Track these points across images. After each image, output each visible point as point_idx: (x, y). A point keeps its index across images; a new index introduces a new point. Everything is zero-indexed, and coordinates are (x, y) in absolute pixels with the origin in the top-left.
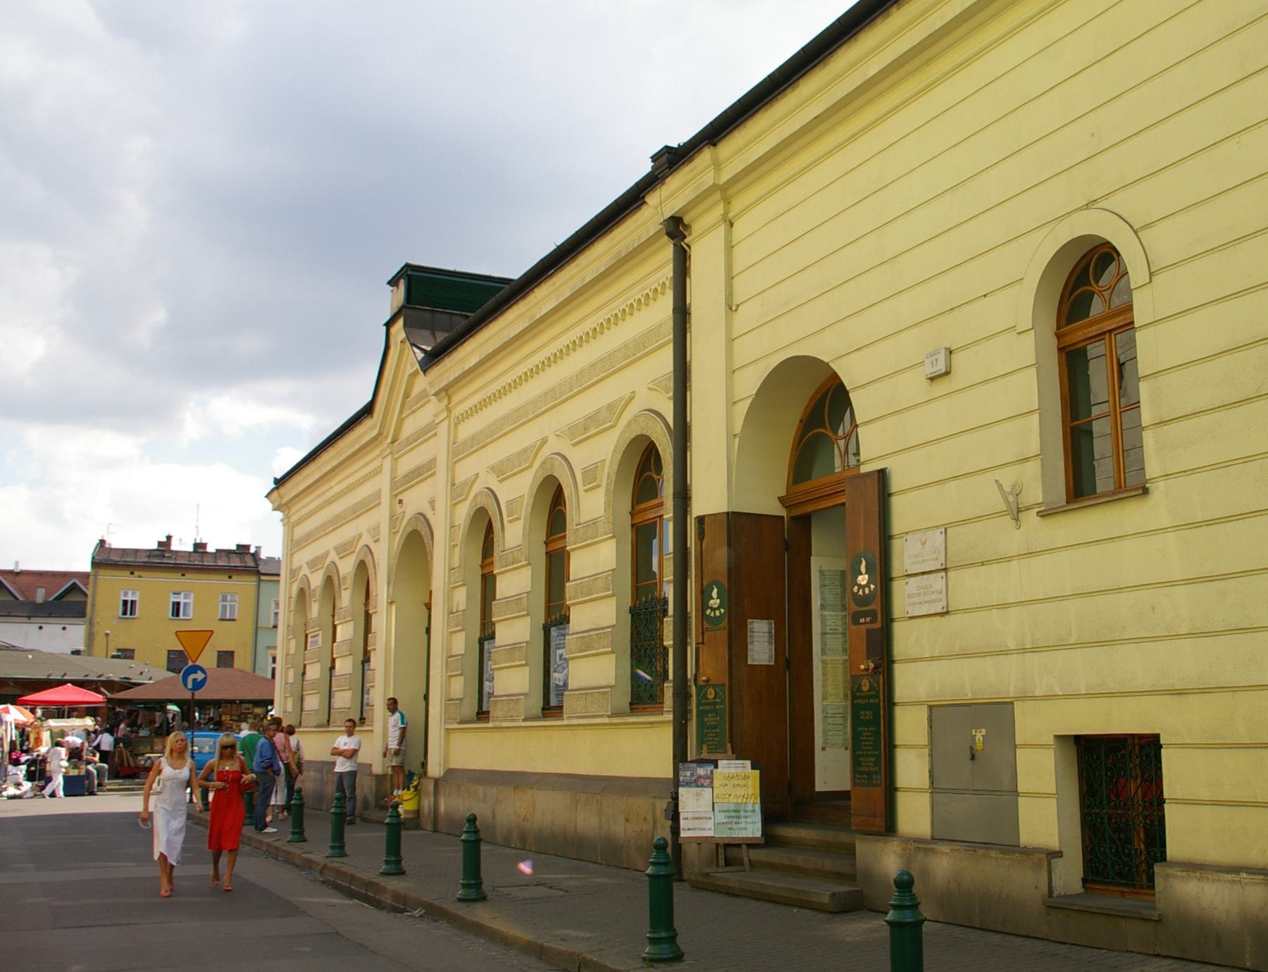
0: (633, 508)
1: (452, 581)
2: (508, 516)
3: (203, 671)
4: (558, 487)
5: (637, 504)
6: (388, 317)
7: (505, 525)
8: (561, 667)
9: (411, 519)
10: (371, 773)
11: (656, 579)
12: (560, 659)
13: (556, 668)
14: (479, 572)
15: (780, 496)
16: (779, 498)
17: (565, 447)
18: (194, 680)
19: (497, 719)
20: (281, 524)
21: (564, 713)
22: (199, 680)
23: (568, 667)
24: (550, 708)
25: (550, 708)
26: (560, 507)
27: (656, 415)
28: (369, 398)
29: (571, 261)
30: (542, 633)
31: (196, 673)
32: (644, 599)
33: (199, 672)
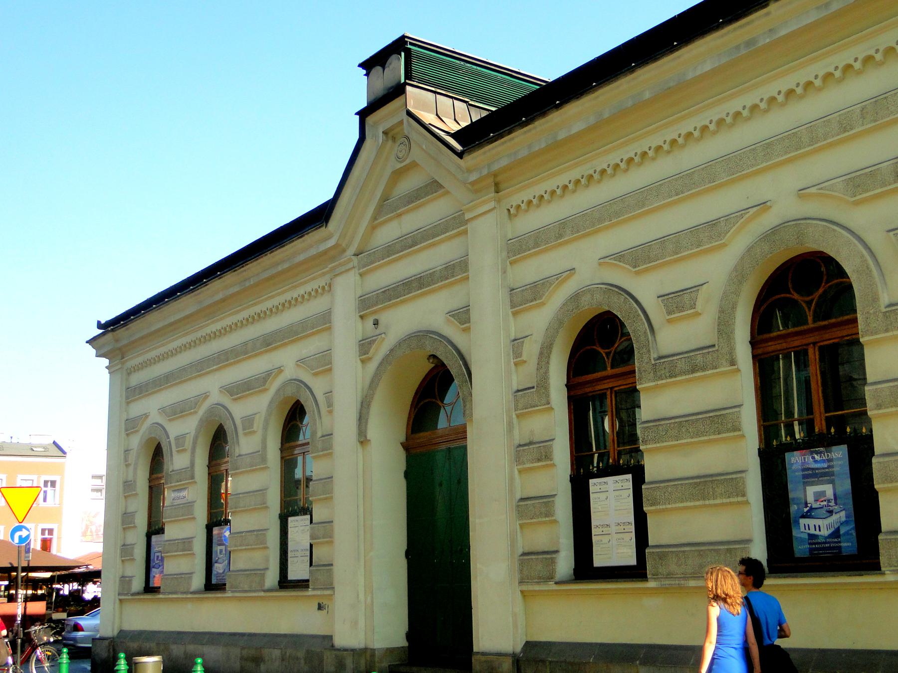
0: (150, 477)
1: (520, 406)
2: (244, 429)
3: (28, 530)
4: (158, 445)
5: (574, 377)
6: (363, 104)
7: (173, 454)
8: (158, 565)
9: (400, 344)
10: (333, 646)
11: (223, 508)
12: (157, 560)
13: (218, 560)
14: (147, 485)
15: (401, 442)
16: (401, 443)
17: (226, 400)
18: (20, 537)
19: (164, 593)
20: (107, 371)
21: (310, 585)
22: (23, 537)
23: (163, 565)
24: (212, 586)
25: (212, 586)
26: (295, 422)
27: (299, 382)
28: (330, 196)
29: (551, 110)
30: (145, 539)
31: (21, 530)
32: (291, 509)
33: (24, 530)
